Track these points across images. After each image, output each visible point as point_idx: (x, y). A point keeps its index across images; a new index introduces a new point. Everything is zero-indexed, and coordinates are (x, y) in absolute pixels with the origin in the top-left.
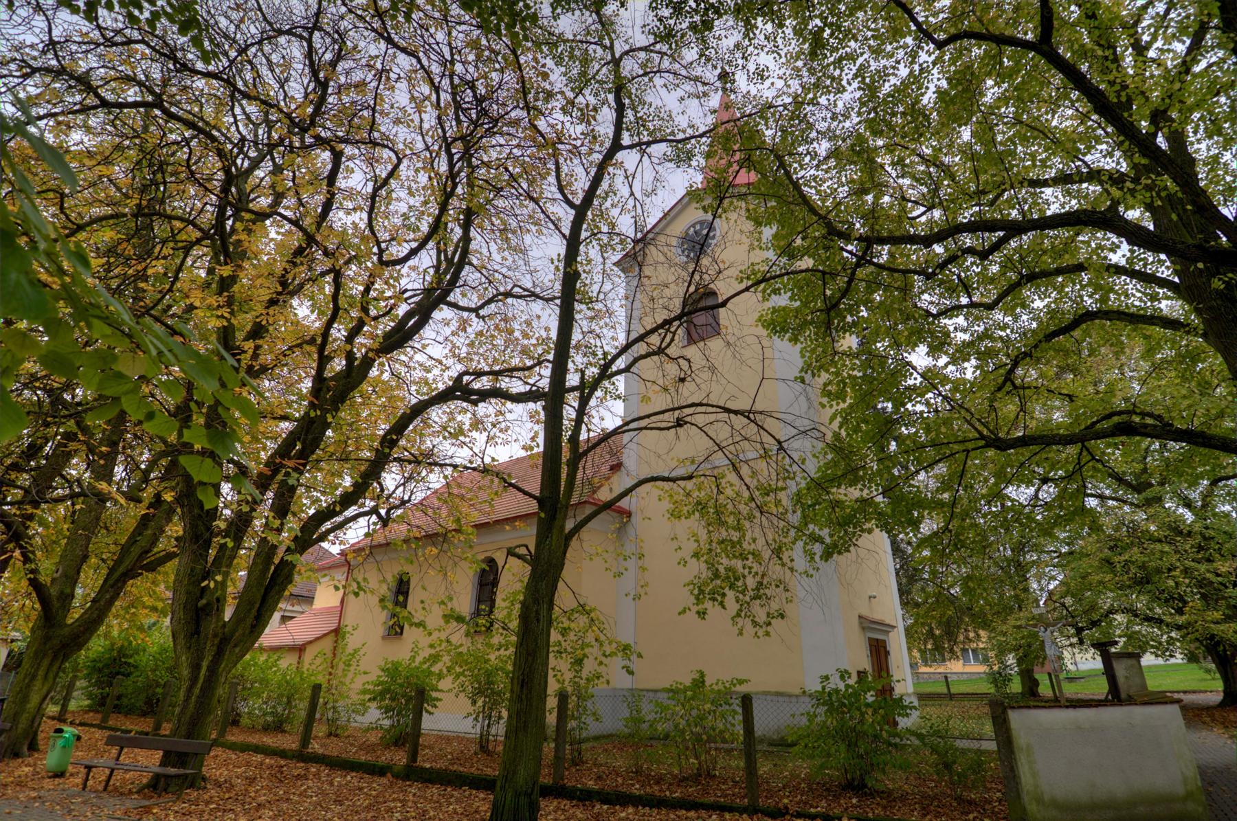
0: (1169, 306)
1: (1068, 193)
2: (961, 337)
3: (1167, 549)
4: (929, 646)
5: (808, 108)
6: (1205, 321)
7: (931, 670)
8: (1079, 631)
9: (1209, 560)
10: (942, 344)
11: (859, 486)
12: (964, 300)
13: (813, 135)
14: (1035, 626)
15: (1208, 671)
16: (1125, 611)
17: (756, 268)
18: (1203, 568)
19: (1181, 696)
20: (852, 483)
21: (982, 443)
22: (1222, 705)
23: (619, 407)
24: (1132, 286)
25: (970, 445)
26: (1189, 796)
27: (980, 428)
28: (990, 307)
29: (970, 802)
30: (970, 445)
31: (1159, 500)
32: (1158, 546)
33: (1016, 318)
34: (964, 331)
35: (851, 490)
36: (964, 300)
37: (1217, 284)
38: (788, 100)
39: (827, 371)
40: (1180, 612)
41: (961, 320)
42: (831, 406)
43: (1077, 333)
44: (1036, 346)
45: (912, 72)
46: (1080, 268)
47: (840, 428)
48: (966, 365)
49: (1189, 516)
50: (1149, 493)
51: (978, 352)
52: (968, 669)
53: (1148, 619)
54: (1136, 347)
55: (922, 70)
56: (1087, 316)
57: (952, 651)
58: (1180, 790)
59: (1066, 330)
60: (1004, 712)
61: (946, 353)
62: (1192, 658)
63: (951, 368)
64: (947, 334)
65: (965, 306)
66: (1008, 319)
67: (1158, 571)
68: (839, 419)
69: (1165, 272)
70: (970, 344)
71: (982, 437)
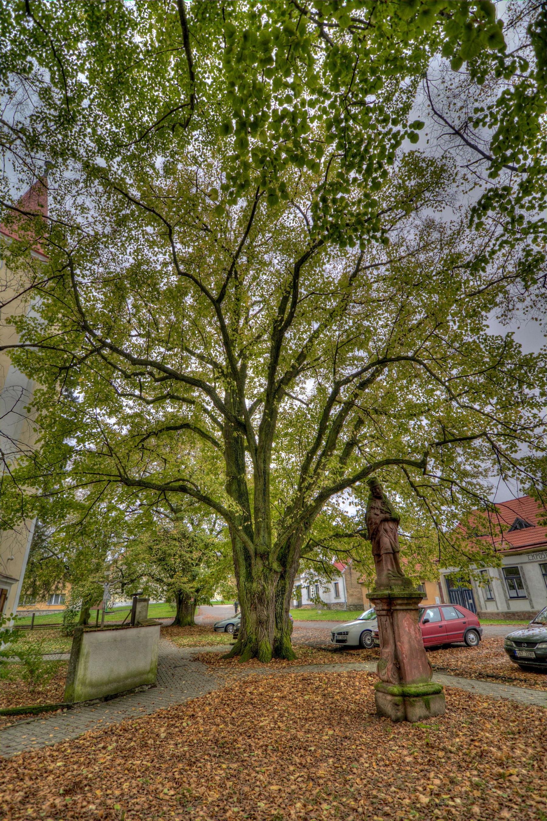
0: (218, 434)
1: (201, 364)
2: (129, 411)
3: (177, 544)
4: (29, 593)
5: (101, 246)
6: (227, 448)
7: (25, 609)
8: (124, 585)
9: (191, 552)
10: (117, 411)
11: (37, 486)
12: (137, 392)
13: (97, 261)
14: (103, 582)
15: (172, 607)
16: (149, 575)
17: (24, 319)
18: (188, 555)
19: (161, 621)
20: (33, 485)
21: (119, 479)
22: (172, 625)
23: (141, 581)
24: (208, 420)
25: (112, 478)
26: (150, 671)
27: (122, 470)
28: (148, 403)
29: (39, 693)
30: (112, 478)
31: (182, 519)
32: (174, 542)
33: (157, 412)
34: (131, 408)
35: (30, 488)
36: (137, 392)
37: (235, 434)
38: (92, 233)
39: (48, 410)
40: (172, 577)
41: (131, 403)
42: (41, 432)
43: (180, 432)
44: (160, 431)
45: (162, 270)
46: (193, 402)
47: (41, 448)
48: (124, 427)
49: (191, 529)
50: (178, 515)
51: (133, 423)
52: (52, 608)
53: (157, 580)
54: (199, 445)
55: (166, 273)
56: (186, 426)
57: (44, 596)
58: (148, 668)
59: (176, 428)
60: (82, 635)
61: (116, 417)
62: (168, 601)
63: (116, 427)
64: (121, 407)
65: (136, 396)
66: (152, 411)
67: (170, 555)
68: (43, 442)
69: (220, 419)
70: (131, 417)
71: (120, 476)
